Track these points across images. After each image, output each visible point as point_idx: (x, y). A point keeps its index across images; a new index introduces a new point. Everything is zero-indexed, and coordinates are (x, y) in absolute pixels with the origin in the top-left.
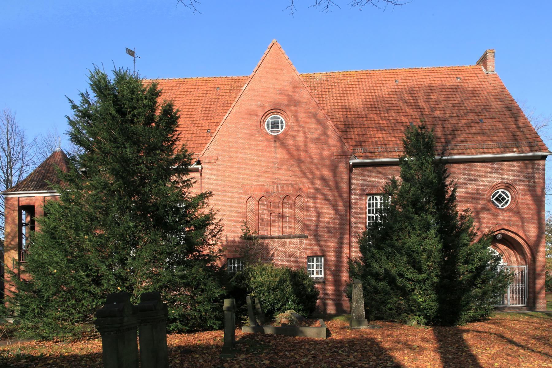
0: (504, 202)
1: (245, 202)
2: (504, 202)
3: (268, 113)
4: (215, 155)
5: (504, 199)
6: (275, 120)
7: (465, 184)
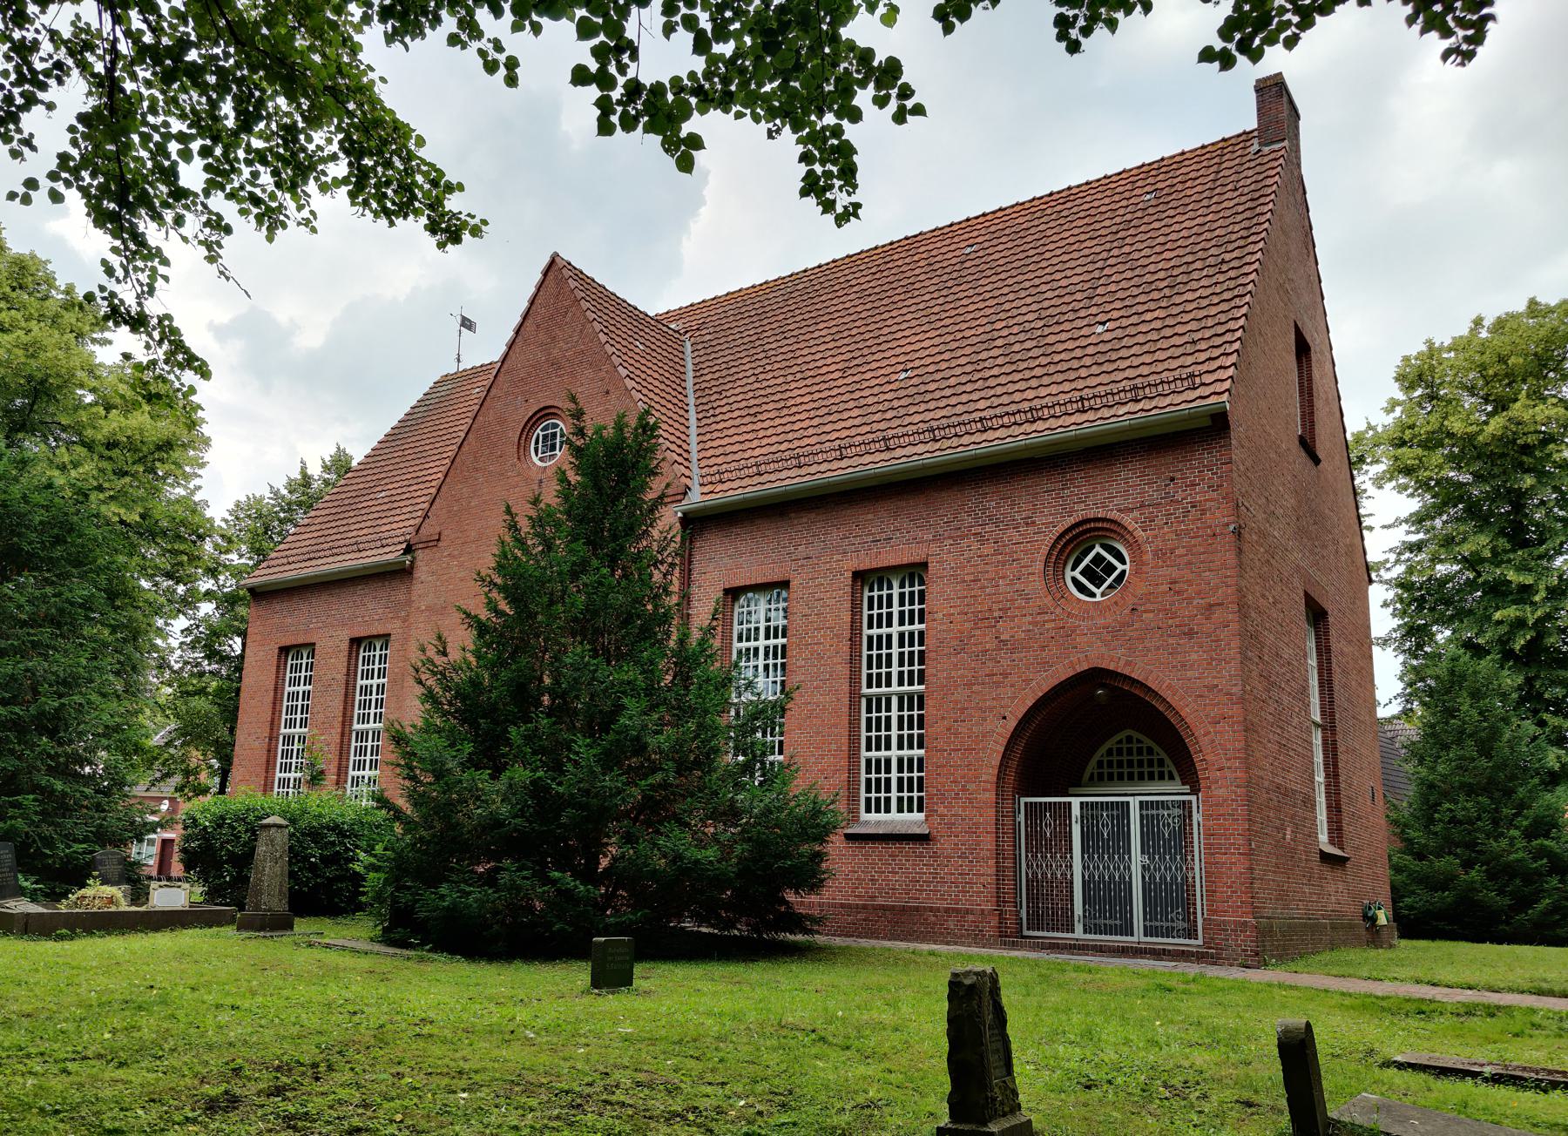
5: (1110, 569)
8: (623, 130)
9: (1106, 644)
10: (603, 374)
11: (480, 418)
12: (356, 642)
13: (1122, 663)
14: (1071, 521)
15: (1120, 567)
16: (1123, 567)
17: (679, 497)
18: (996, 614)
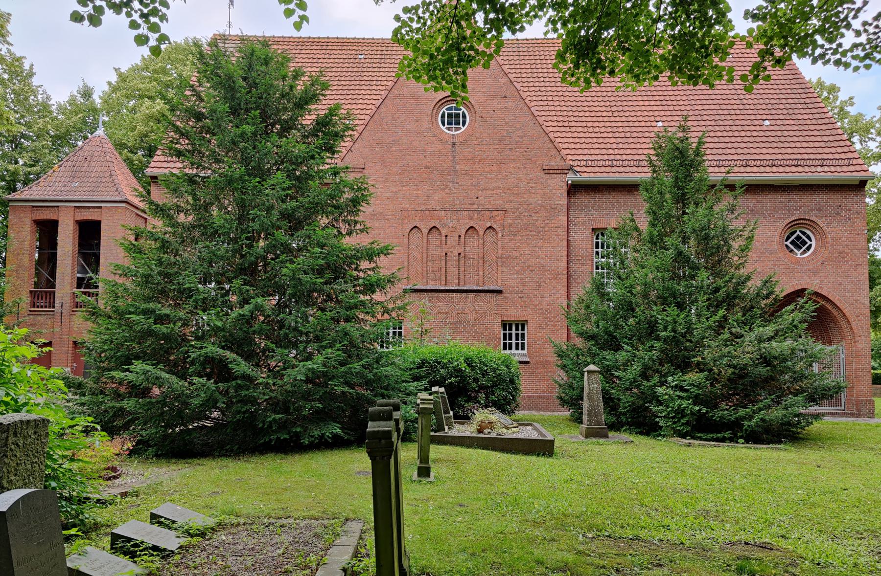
0: (804, 248)
1: (406, 235)
2: (804, 248)
3: (443, 101)
4: (362, 161)
5: (804, 243)
6: (454, 111)
7: (726, 186)
8: (136, 36)
9: (810, 277)
10: (501, 84)
11: (395, 91)
12: (490, 227)
13: (817, 287)
14: (793, 218)
15: (809, 243)
16: (786, 243)
17: (565, 171)
18: (755, 259)
